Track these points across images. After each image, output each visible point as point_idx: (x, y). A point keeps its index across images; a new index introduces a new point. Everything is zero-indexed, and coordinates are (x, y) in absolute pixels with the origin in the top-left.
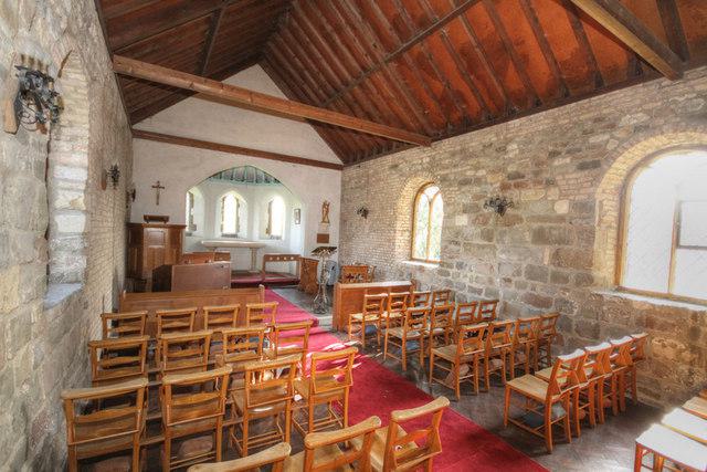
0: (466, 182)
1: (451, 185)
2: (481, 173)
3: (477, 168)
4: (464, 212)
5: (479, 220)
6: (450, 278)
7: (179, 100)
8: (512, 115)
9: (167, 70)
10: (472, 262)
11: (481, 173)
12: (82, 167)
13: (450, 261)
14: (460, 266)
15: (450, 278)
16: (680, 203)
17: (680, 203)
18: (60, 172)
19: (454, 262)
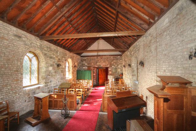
0: (51, 58)
1: (47, 57)
2: (54, 56)
3: (54, 55)
4: (51, 66)
5: (54, 69)
6: (49, 86)
7: (94, 42)
8: (31, 32)
9: (150, 127)
10: (52, 79)
11: (54, 56)
12: (33, 57)
13: (48, 81)
14: (51, 82)
15: (49, 86)
16: (157, 76)
17: (157, 76)
18: (52, 32)
19: (49, 81)
